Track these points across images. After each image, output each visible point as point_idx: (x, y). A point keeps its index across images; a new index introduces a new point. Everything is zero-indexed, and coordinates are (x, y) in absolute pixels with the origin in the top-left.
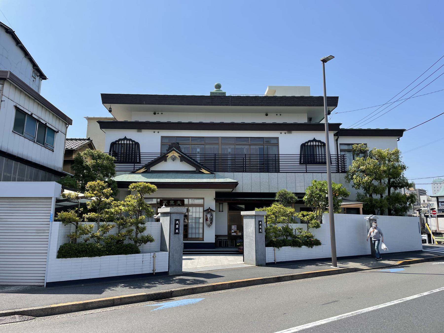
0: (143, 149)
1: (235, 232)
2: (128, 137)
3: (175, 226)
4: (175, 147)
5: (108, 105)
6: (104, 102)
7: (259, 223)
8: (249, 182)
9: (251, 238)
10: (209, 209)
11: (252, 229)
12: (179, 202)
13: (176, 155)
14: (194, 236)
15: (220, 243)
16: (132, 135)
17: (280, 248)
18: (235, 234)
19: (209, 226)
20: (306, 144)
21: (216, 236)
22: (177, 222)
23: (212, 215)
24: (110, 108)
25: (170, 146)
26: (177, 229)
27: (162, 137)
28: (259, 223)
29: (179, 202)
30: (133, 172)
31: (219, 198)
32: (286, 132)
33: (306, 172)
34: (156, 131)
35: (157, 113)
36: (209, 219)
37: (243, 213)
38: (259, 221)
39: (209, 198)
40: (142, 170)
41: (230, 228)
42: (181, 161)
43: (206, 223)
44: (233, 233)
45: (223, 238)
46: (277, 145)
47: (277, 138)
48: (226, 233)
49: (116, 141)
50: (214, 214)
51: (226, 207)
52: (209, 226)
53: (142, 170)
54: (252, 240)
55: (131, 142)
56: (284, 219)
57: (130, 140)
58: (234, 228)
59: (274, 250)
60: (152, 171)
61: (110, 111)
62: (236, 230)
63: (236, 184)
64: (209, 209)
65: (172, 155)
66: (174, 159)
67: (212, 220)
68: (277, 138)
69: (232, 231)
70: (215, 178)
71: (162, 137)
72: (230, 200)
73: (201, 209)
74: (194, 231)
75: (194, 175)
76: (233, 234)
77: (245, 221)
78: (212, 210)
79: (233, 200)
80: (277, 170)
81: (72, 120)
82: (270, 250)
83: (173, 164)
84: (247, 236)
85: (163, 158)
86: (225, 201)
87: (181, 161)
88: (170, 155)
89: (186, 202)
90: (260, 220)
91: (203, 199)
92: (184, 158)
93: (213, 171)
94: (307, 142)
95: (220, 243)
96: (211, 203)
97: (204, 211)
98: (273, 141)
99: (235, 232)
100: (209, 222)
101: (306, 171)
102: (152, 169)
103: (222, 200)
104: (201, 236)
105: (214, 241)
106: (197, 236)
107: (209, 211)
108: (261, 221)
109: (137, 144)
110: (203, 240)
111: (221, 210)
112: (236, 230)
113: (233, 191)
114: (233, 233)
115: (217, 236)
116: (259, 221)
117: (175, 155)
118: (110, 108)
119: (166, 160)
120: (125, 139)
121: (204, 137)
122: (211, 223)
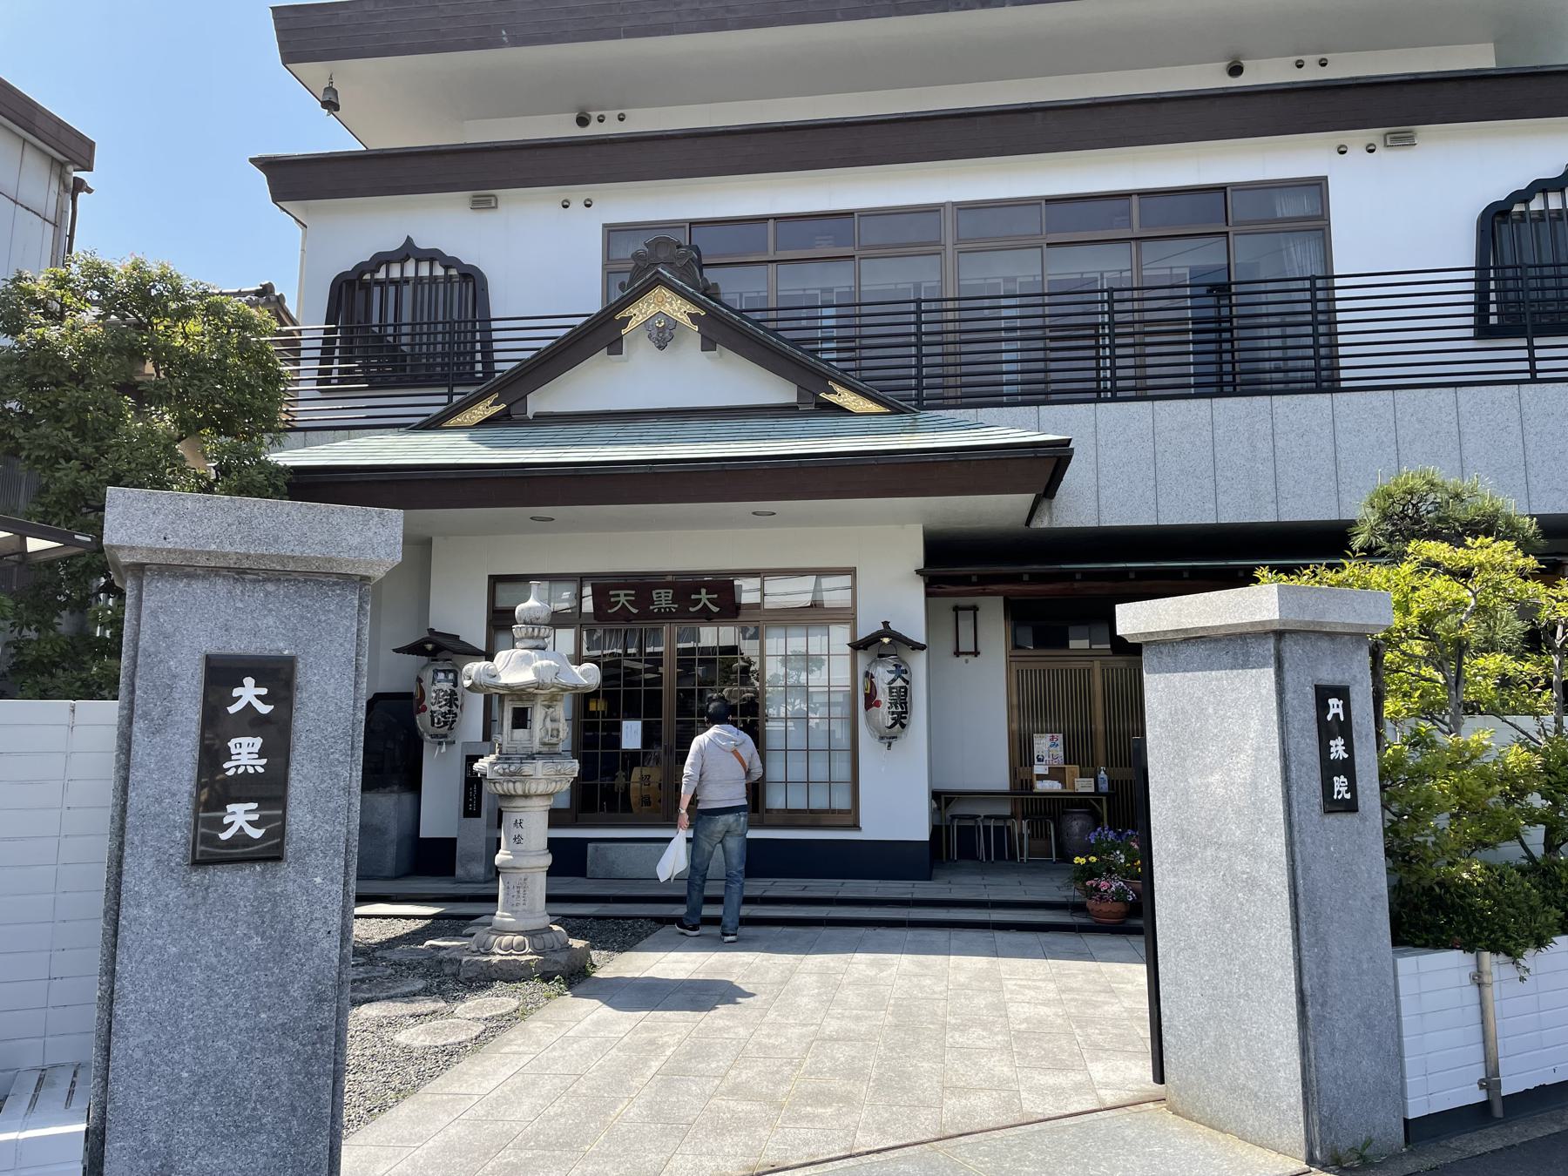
0: (504, 301)
1: (1056, 773)
2: (422, 243)
3: (212, 755)
4: (669, 264)
5: (317, 71)
6: (291, 55)
7: (1322, 707)
8: (1134, 461)
9: (1242, 864)
10: (886, 630)
11: (1242, 775)
12: (704, 596)
13: (678, 309)
14: (797, 801)
15: (967, 834)
16: (445, 225)
17: (1530, 957)
18: (1055, 786)
19: (888, 739)
20: (1518, 208)
21: (936, 795)
22: (248, 693)
23: (901, 671)
24: (330, 89)
25: (646, 260)
26: (244, 788)
27: (611, 231)
28: (1322, 707)
29: (704, 596)
30: (433, 424)
31: (950, 564)
32: (1373, 135)
33: (1534, 380)
34: (577, 193)
35: (594, 115)
36: (883, 697)
37: (1132, 619)
38: (1323, 694)
39: (878, 562)
40: (482, 411)
41: (1022, 753)
42: (708, 344)
43: (867, 718)
44: (1041, 777)
45: (983, 810)
46: (1317, 227)
47: (1318, 186)
48: (999, 779)
49: (361, 268)
50: (918, 664)
51: (994, 632)
52: (888, 739)
53: (482, 411)
54: (1252, 884)
55: (439, 271)
56: (1505, 682)
57: (433, 256)
58: (1048, 748)
59: (1478, 980)
60: (536, 416)
61: (331, 105)
62: (1059, 762)
63: (1050, 463)
64: (886, 630)
65: (652, 310)
66: (664, 335)
67: (902, 700)
68: (1318, 186)
69: (1039, 769)
70: (914, 430)
71: (611, 231)
72: (1015, 579)
73: (840, 636)
74: (797, 770)
75: (798, 424)
76: (1043, 786)
77: (1164, 692)
78: (898, 639)
79: (1036, 578)
80: (1324, 378)
81: (91, 145)
82: (1436, 978)
83: (670, 377)
84: (1182, 834)
85: (598, 335)
86: (985, 583)
87: (708, 344)
88: (640, 312)
89: (748, 592)
90: (1328, 676)
91: (852, 572)
92: (725, 329)
93: (906, 398)
94: (1524, 196)
95: (967, 834)
96: (903, 603)
97: (856, 646)
98: (1287, 207)
99: (1056, 773)
100: (884, 714)
101: (1533, 371)
102: (541, 401)
103: (964, 580)
104: (841, 801)
105: (920, 832)
106: (819, 801)
107: (880, 644)
108: (1342, 693)
109: (472, 279)
110: (856, 826)
111: (966, 644)
112: (1059, 762)
113: (1042, 523)
114: (1041, 777)
115: (941, 798)
116: (1323, 694)
117: (667, 309)
118: (330, 89)
119: (615, 347)
120: (408, 251)
121: (848, 214)
122: (901, 719)
